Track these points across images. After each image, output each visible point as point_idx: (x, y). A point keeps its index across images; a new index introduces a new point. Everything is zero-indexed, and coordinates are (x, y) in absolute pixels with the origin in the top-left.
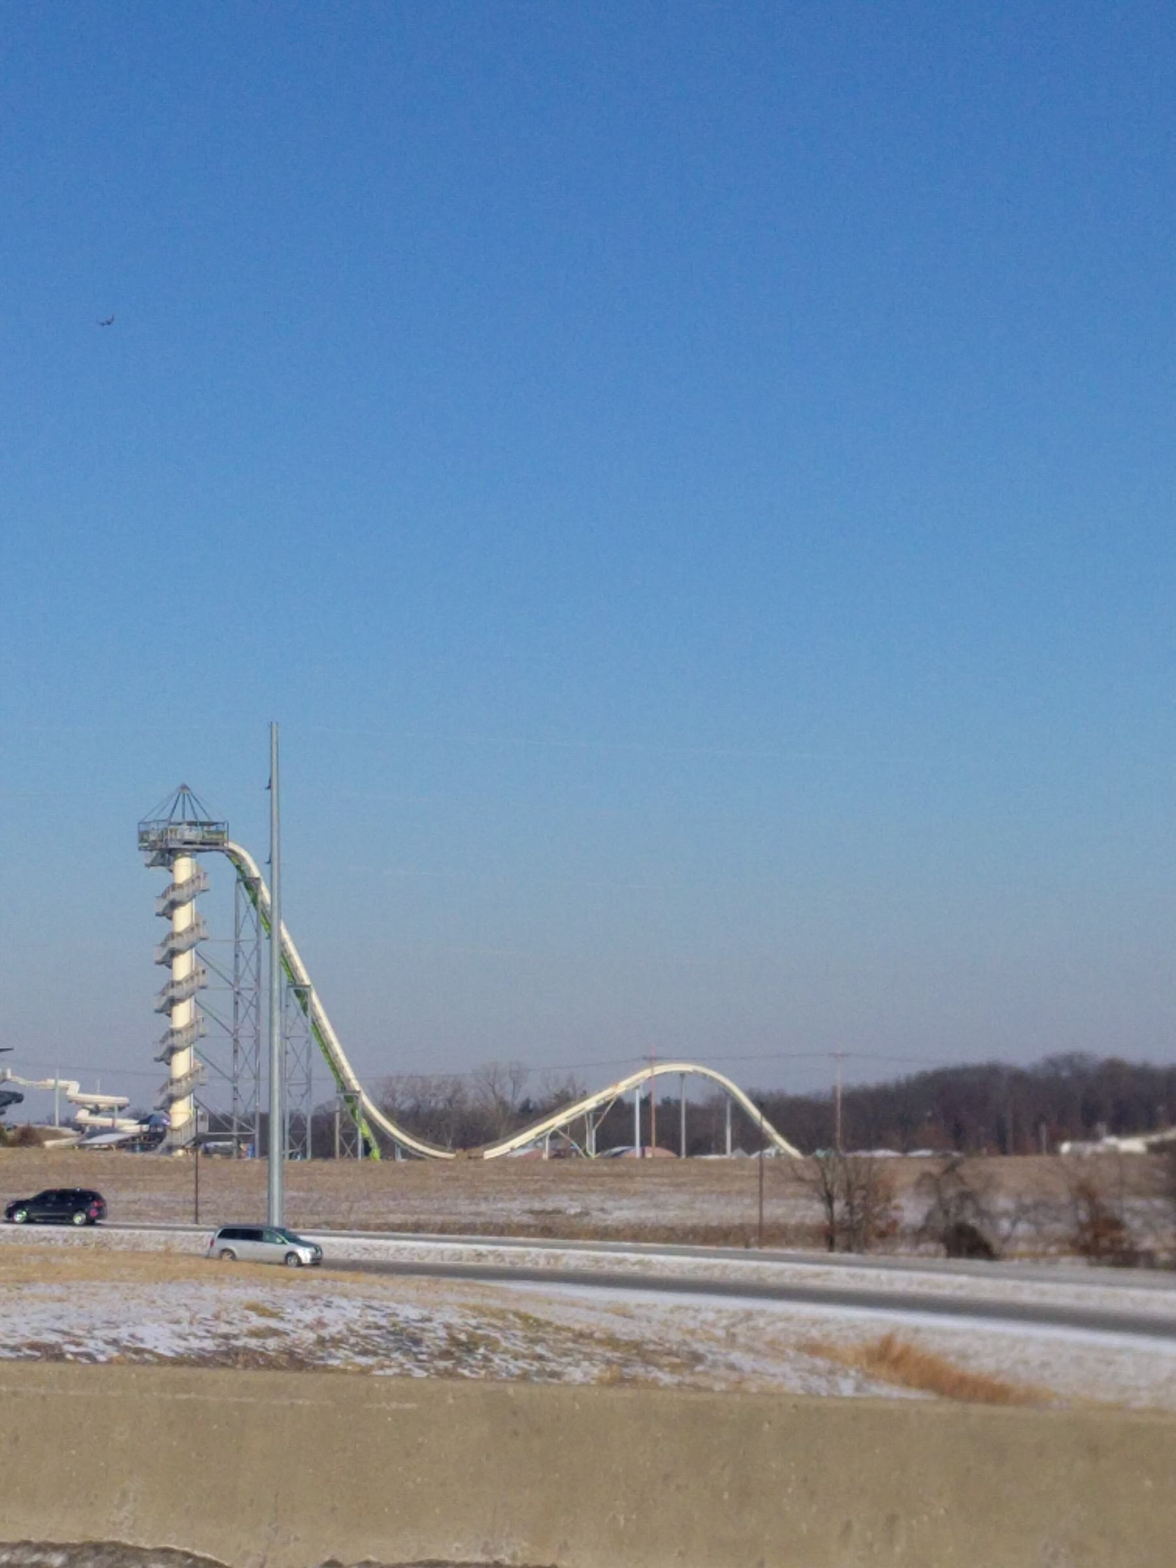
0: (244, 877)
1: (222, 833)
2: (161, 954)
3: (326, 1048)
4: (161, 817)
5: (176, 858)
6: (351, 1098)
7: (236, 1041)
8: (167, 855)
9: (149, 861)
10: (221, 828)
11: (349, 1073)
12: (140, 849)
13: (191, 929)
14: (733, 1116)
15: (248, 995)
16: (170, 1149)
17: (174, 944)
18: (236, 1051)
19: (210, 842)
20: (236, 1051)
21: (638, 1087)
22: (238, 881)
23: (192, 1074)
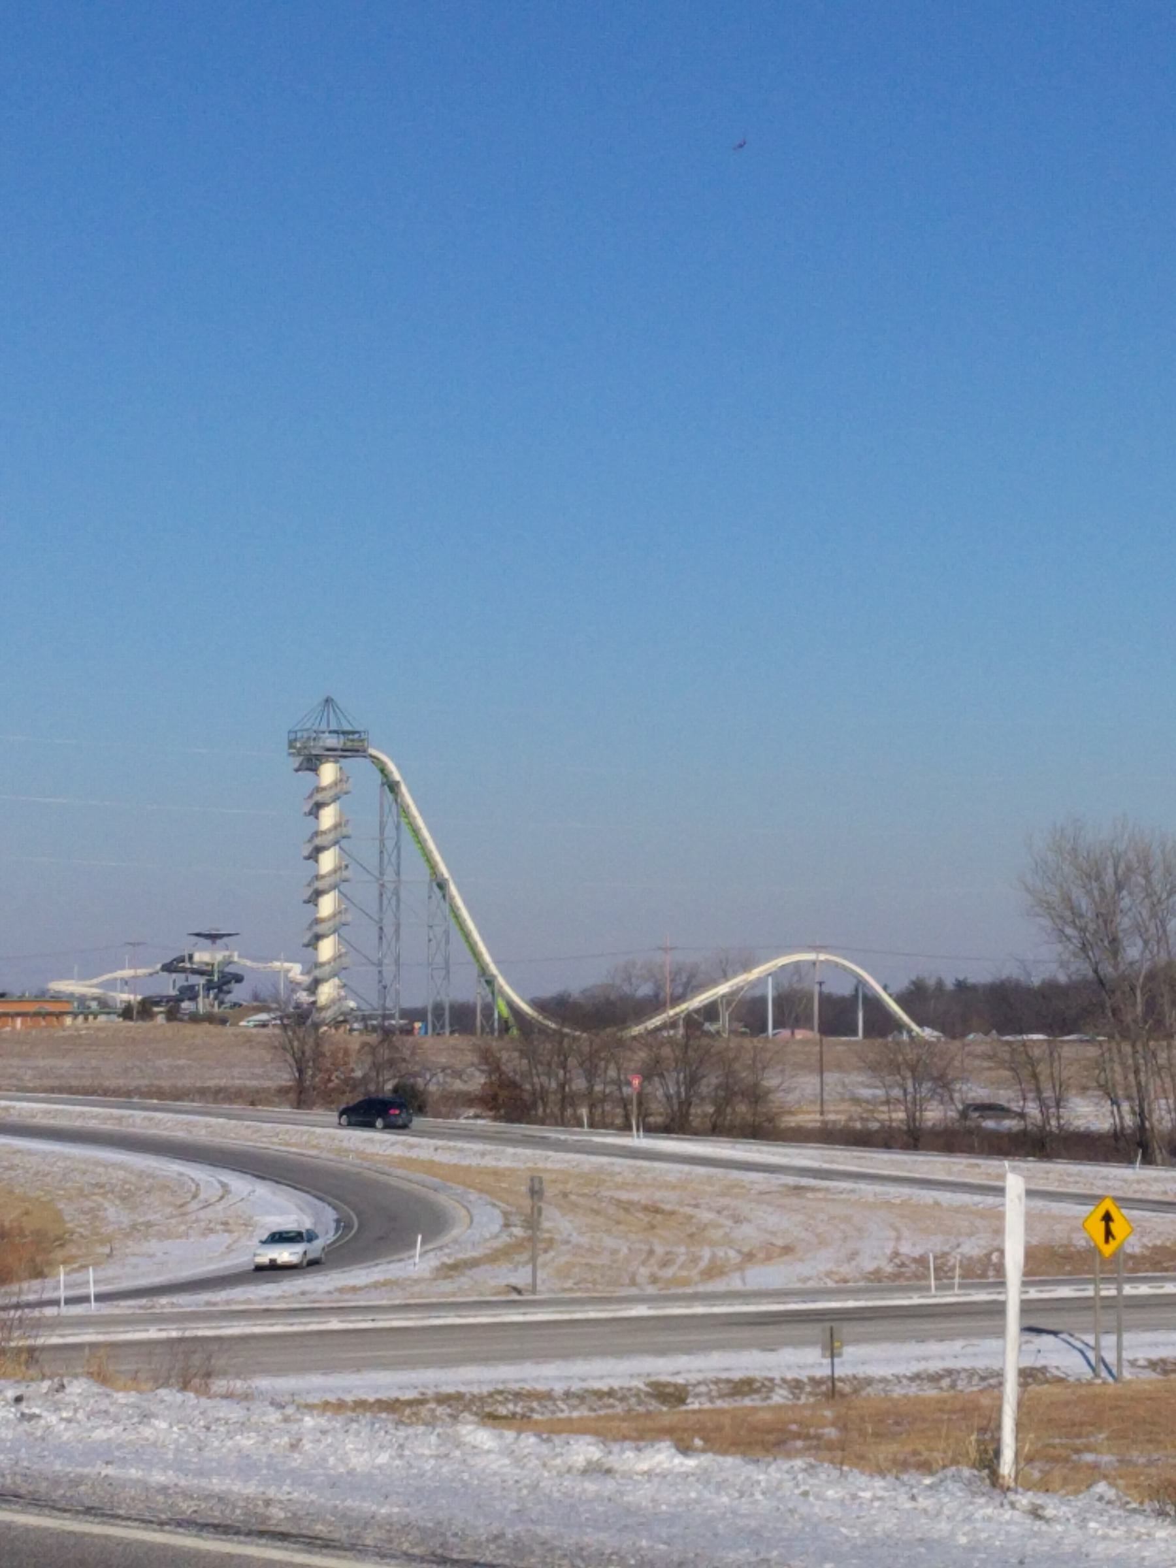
0: (388, 780)
1: (362, 741)
2: (306, 850)
3: (467, 936)
4: (308, 726)
5: (322, 763)
6: (490, 982)
7: (381, 929)
8: (311, 763)
9: (296, 765)
10: (363, 736)
11: (487, 958)
12: (290, 754)
13: (336, 826)
14: (863, 1003)
15: (390, 886)
17: (318, 841)
18: (381, 938)
19: (352, 748)
20: (381, 938)
22: (383, 784)
23: (338, 957)
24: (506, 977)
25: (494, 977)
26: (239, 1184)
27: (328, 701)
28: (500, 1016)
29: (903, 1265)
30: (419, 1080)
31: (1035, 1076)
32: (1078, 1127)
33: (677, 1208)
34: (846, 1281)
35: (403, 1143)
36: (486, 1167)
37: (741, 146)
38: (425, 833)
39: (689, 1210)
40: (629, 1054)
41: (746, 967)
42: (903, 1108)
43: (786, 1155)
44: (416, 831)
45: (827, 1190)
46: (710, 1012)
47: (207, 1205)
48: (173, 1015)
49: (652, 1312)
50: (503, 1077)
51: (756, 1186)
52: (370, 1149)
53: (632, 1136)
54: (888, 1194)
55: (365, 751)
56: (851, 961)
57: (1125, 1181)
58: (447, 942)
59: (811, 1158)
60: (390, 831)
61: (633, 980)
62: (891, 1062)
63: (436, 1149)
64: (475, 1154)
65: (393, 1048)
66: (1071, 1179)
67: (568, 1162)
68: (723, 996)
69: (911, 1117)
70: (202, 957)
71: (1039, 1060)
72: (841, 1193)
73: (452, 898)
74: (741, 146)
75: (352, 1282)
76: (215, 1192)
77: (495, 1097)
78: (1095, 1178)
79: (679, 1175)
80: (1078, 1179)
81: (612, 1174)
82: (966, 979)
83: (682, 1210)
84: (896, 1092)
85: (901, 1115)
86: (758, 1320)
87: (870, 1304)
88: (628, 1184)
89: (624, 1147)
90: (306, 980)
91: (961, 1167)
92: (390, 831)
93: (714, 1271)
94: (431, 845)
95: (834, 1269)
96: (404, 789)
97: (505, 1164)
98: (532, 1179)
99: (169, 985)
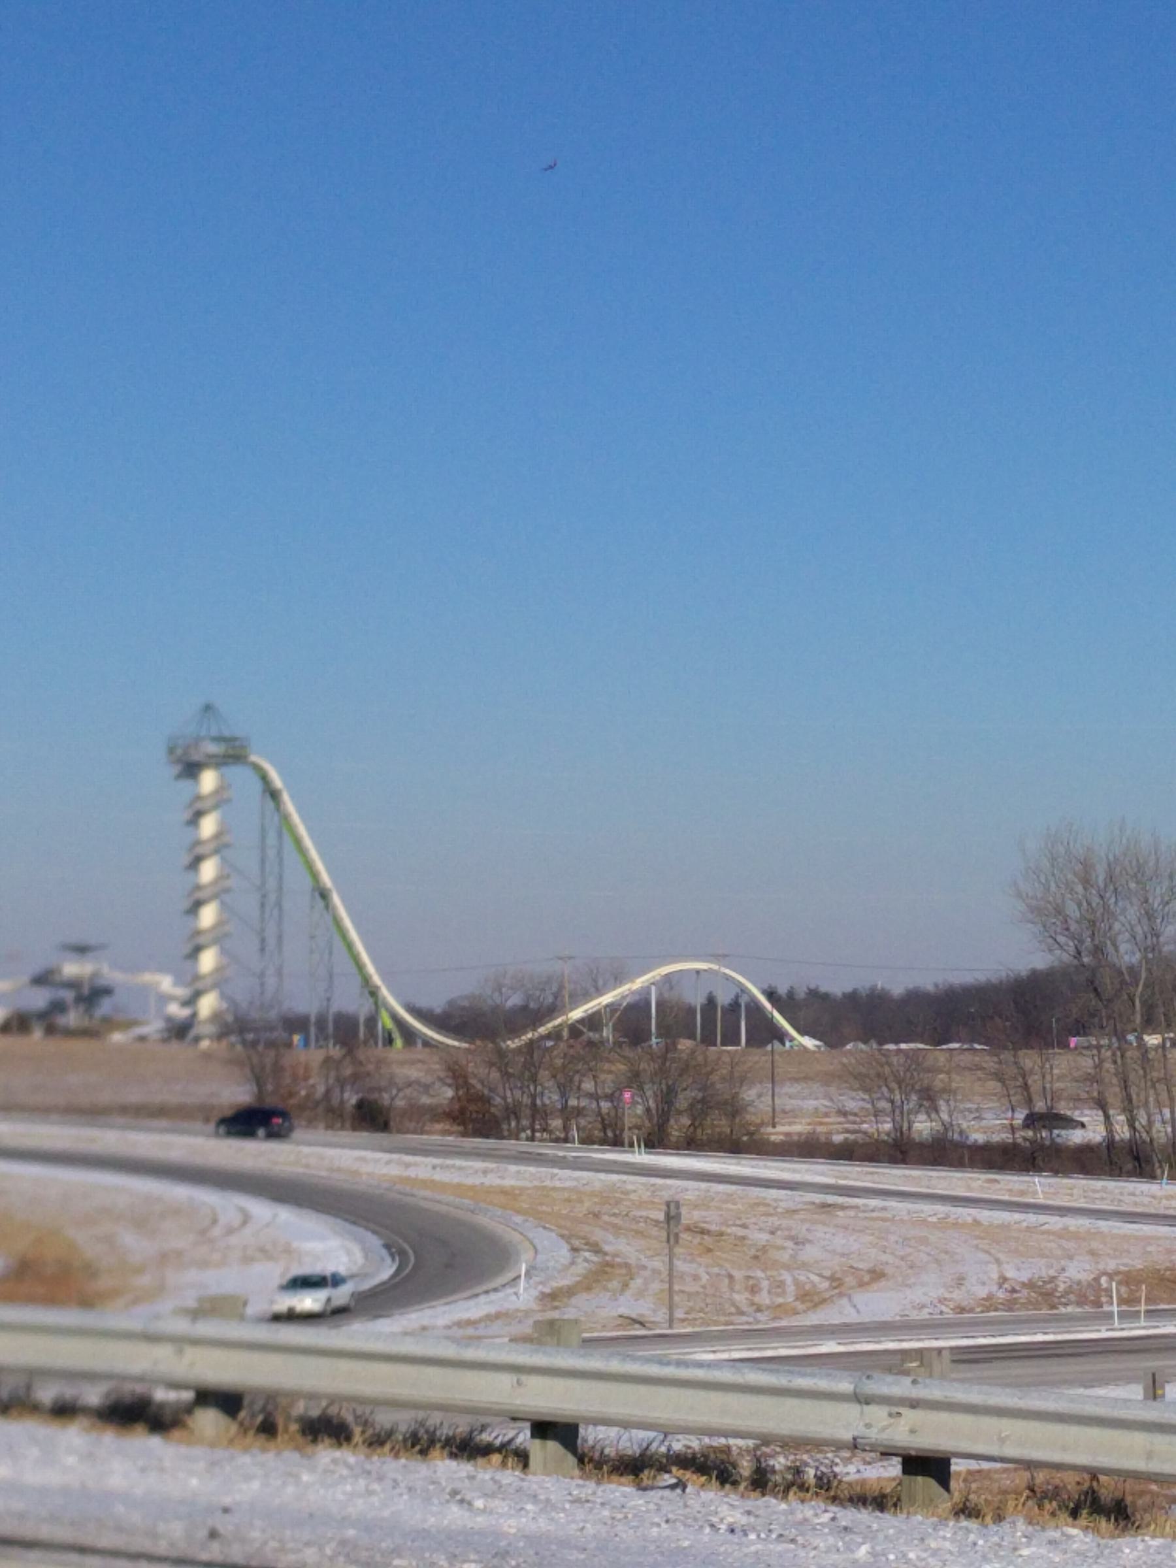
3: (350, 946)
6: (374, 993)
8: (191, 770)
11: (371, 969)
16: (197, 1039)
19: (233, 755)
21: (653, 984)
24: (389, 987)
25: (378, 988)
26: (260, 1209)
27: (208, 708)
28: (383, 1027)
29: (1014, 1291)
30: (386, 1096)
31: (1026, 1087)
32: (976, 1141)
33: (724, 1229)
34: (962, 1310)
35: (399, 1163)
36: (491, 1186)
37: (551, 167)
38: (308, 842)
39: (741, 1232)
40: (607, 1066)
41: (618, 978)
42: (889, 1119)
43: (794, 1171)
44: (298, 842)
45: (856, 1207)
46: (593, 1021)
47: (230, 1231)
48: (51, 1030)
49: (842, 1349)
50: (472, 1091)
51: (781, 1204)
52: (365, 1169)
53: (633, 1152)
54: (922, 1211)
55: (245, 757)
56: (734, 971)
57: (1154, 1197)
58: (331, 953)
59: (823, 1174)
60: (272, 840)
61: (504, 990)
62: (879, 1075)
63: (434, 1167)
64: (476, 1172)
65: (358, 1063)
66: (1097, 1195)
67: (576, 1179)
68: (607, 1006)
69: (898, 1129)
70: (72, 969)
71: (1031, 1072)
72: (873, 1211)
73: (334, 909)
74: (551, 167)
75: (465, 1316)
76: (237, 1220)
77: (462, 1111)
78: (1121, 1194)
79: (697, 1193)
80: (1105, 1195)
81: (626, 1193)
82: (817, 987)
83: (729, 1230)
84: (883, 1105)
85: (888, 1126)
86: (965, 1357)
87: (1060, 1337)
88: (645, 1202)
89: (627, 1164)
90: (182, 992)
91: (980, 1182)
92: (272, 840)
93: (810, 1298)
94: (314, 854)
95: (947, 1295)
96: (286, 797)
97: (509, 1182)
98: (668, 1204)
99: (39, 999)
